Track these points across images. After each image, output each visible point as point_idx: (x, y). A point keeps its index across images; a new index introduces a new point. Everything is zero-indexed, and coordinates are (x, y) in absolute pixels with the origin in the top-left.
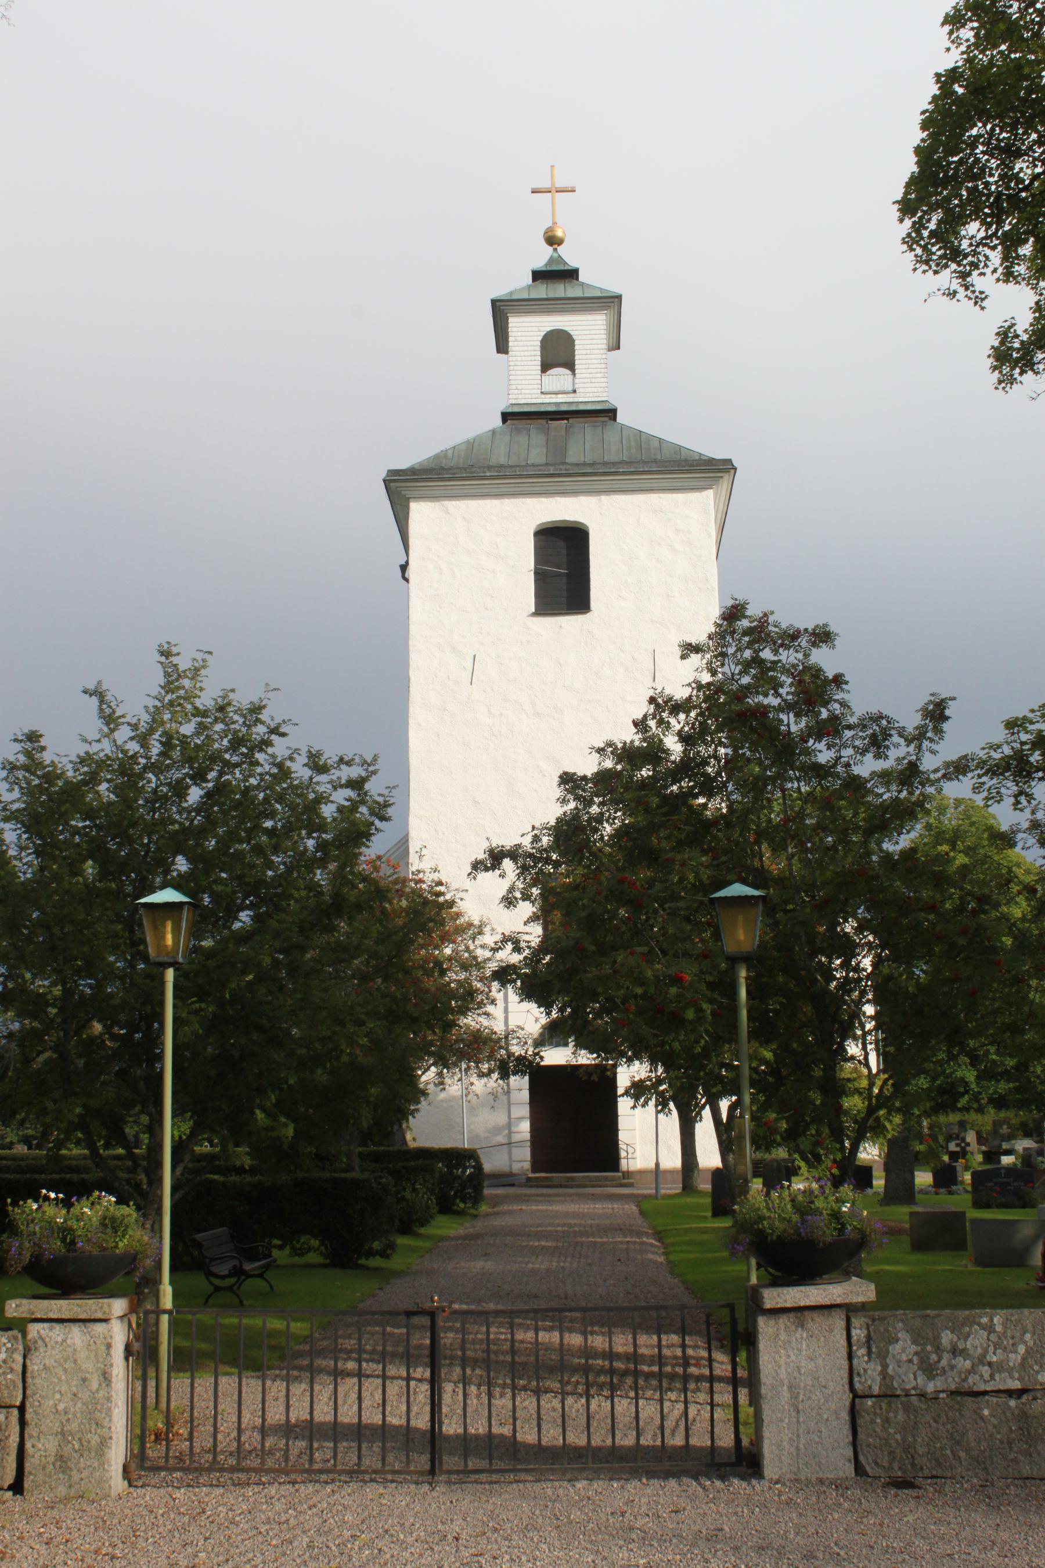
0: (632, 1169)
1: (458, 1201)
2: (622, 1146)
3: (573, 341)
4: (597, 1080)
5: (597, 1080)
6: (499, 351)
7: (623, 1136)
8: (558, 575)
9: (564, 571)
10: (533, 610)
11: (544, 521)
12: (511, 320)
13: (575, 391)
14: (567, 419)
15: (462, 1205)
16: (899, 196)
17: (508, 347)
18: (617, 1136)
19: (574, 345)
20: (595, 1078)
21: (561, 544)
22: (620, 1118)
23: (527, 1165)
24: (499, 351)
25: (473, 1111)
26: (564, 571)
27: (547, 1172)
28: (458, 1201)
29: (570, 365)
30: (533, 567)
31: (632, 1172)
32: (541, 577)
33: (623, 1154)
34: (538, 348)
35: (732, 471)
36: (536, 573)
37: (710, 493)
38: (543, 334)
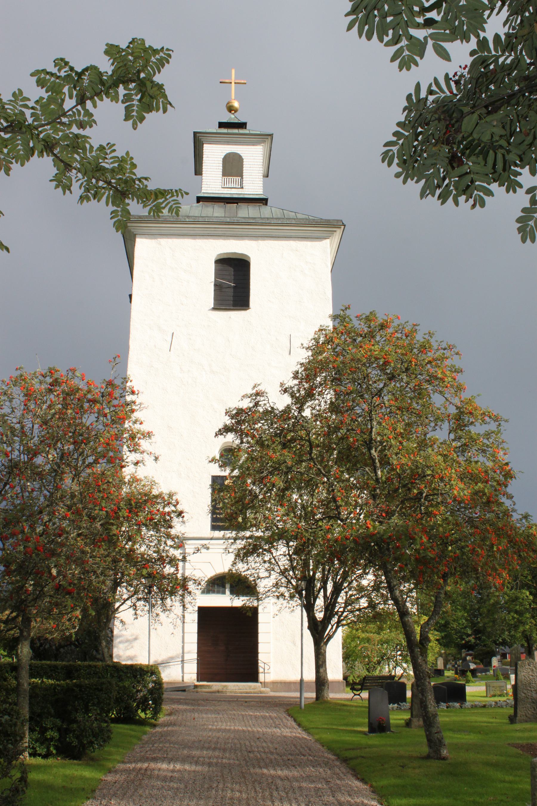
0: (267, 680)
1: (139, 711)
2: (261, 664)
3: (243, 159)
4: (250, 615)
5: (250, 615)
6: (196, 174)
7: (262, 657)
8: (230, 287)
9: (234, 284)
10: (213, 306)
11: (222, 252)
12: (205, 145)
13: (242, 188)
14: (237, 203)
15: (143, 715)
16: (330, 312)
17: (202, 171)
18: (257, 656)
19: (243, 162)
20: (250, 614)
21: (231, 270)
22: (196, 631)
23: (195, 676)
24: (196, 174)
25: (156, 639)
26: (234, 284)
27: (208, 681)
28: (139, 711)
29: (240, 174)
30: (213, 280)
31: (267, 683)
32: (218, 287)
33: (261, 670)
34: (221, 162)
35: (343, 227)
36: (215, 285)
37: (328, 241)
38: (224, 154)
